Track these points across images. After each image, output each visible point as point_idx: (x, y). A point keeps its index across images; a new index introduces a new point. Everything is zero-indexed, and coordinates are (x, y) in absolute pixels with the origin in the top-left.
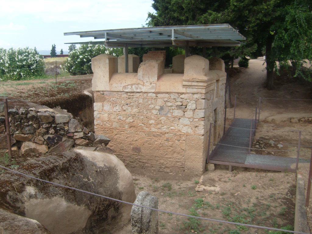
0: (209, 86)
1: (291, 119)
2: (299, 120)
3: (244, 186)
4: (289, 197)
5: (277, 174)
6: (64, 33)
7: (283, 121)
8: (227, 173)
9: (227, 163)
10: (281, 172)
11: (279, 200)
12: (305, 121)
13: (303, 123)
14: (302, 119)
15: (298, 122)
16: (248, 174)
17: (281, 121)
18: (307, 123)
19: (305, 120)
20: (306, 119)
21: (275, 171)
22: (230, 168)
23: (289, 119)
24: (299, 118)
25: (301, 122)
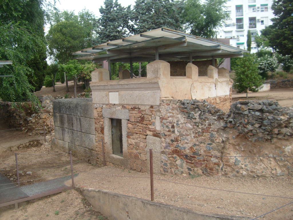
0: (165, 98)
1: (11, 148)
2: (18, 147)
3: (47, 216)
4: (89, 209)
5: (59, 195)
6: (110, 80)
7: (5, 152)
8: (16, 212)
9: (12, 203)
10: (61, 192)
11: (86, 214)
12: (24, 147)
13: (22, 149)
14: (20, 146)
15: (17, 149)
16: (35, 205)
17: (3, 152)
18: (26, 148)
19: (24, 146)
20: (24, 145)
21: (54, 195)
22: (16, 206)
23: (9, 149)
24: (17, 146)
25: (20, 149)
